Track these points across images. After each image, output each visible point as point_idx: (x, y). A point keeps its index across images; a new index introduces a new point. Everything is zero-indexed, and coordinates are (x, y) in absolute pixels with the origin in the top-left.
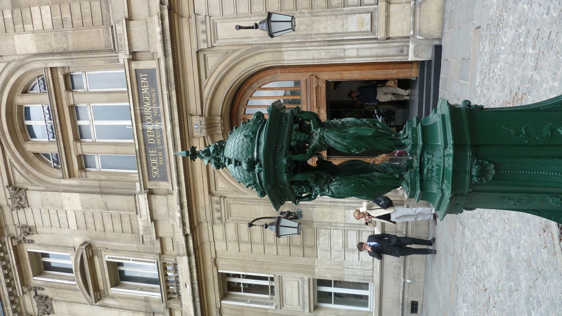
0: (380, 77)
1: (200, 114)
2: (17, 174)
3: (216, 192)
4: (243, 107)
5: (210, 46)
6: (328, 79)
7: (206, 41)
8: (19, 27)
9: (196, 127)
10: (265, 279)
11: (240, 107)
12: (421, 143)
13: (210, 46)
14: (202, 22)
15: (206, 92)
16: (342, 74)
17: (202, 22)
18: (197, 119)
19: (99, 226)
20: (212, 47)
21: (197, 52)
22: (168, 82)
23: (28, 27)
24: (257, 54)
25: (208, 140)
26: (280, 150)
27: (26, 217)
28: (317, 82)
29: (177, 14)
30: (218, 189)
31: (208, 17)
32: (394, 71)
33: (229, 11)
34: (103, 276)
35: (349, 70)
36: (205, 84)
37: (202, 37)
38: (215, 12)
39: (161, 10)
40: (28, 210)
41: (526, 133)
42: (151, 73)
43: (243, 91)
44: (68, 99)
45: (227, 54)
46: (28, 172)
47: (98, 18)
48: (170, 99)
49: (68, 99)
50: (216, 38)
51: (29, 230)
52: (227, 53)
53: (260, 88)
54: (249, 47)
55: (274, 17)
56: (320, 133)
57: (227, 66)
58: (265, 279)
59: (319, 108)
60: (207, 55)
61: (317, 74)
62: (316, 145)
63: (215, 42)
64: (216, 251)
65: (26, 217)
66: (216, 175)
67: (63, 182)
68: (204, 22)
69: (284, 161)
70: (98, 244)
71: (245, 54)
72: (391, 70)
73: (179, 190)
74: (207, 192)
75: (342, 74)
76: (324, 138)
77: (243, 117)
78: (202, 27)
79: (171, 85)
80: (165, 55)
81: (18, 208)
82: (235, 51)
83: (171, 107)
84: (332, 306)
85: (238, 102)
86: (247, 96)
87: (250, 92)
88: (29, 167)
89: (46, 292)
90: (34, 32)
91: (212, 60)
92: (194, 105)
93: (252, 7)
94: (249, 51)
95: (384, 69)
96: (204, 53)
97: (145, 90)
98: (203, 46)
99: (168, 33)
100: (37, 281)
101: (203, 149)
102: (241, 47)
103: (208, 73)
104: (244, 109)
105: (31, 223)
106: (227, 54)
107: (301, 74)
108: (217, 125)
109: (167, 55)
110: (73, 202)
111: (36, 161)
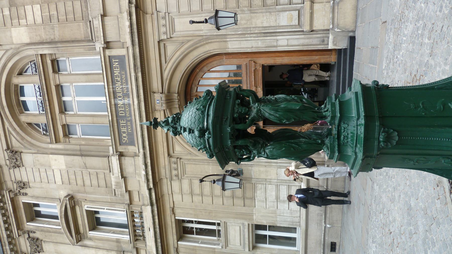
0: (305, 62)
1: (161, 91)
2: (14, 140)
3: (174, 154)
4: (195, 86)
5: (169, 37)
6: (263, 63)
7: (165, 33)
8: (15, 21)
9: (158, 102)
10: (213, 224)
11: (193, 86)
12: (339, 115)
13: (169, 37)
14: (163, 18)
15: (165, 74)
16: (275, 59)
17: (163, 18)
18: (159, 96)
19: (80, 182)
20: (171, 37)
21: (159, 42)
22: (135, 66)
23: (23, 22)
24: (207, 43)
25: (167, 112)
26: (225, 121)
27: (21, 174)
28: (255, 66)
29: (142, 11)
30: (175, 152)
31: (167, 14)
32: (317, 57)
33: (184, 9)
34: (83, 221)
35: (281, 57)
36: (165, 67)
37: (163, 30)
38: (173, 9)
39: (129, 8)
40: (22, 169)
41: (423, 107)
42: (121, 59)
43: (195, 73)
44: (55, 80)
45: (183, 43)
46: (23, 138)
47: (79, 14)
48: (137, 80)
49: (55, 80)
50: (174, 31)
51: (23, 185)
52: (183, 43)
53: (209, 70)
54: (201, 38)
55: (220, 14)
56: (257, 107)
57: (182, 53)
58: (213, 224)
59: (256, 87)
60: (167, 44)
61: (255, 59)
62: (254, 117)
63: (173, 34)
64: (173, 202)
65: (21, 174)
66: (174, 141)
67: (51, 146)
68: (164, 18)
69: (229, 129)
70: (79, 196)
71: (197, 44)
72: (314, 57)
73: (144, 153)
74: (166, 155)
75: (275, 59)
76: (261, 111)
77: (196, 94)
78: (162, 22)
79: (137, 68)
80: (133, 45)
81: (14, 167)
82: (189, 41)
83: (137, 86)
84: (267, 246)
85: (191, 82)
86: (198, 77)
87: (201, 74)
88: (23, 134)
89: (37, 235)
90: (27, 25)
91: (170, 48)
92: (156, 84)
93: (203, 6)
94: (200, 41)
95: (309, 56)
96: (164, 42)
97: (117, 72)
98: (163, 37)
99: (135, 27)
100: (30, 226)
101: (163, 120)
102: (194, 38)
103: (167, 58)
104: (196, 88)
105: (25, 180)
106: (183, 43)
107: (242, 59)
108: (175, 100)
109: (134, 44)
110: (59, 163)
111: (29, 129)
